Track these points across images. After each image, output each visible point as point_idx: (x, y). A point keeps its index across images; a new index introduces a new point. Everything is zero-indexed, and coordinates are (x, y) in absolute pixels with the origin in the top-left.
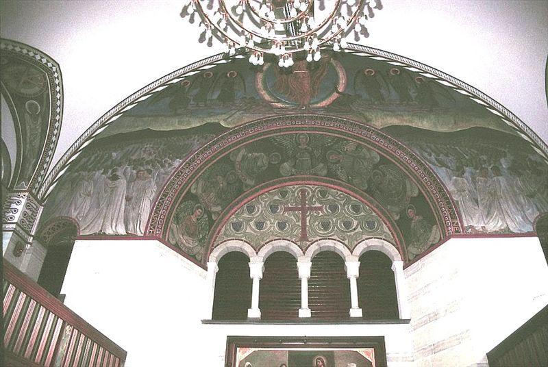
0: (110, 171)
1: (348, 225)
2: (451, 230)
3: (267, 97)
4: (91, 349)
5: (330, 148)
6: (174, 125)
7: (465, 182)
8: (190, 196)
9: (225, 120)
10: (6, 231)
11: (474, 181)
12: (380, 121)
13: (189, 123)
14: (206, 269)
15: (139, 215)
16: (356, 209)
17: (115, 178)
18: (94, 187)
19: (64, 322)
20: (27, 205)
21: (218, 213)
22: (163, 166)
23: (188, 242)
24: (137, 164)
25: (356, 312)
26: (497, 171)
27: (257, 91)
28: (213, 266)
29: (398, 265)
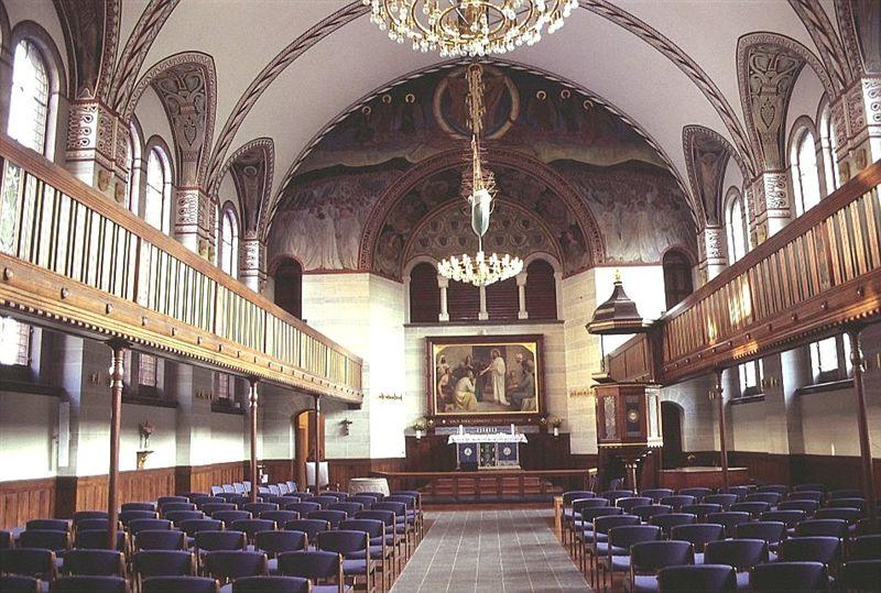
0: (316, 209)
1: (518, 240)
2: (596, 261)
3: (446, 128)
4: (240, 305)
5: (503, 175)
6: (363, 160)
7: (613, 217)
8: (387, 228)
9: (410, 155)
10: (85, 160)
11: (620, 217)
12: (548, 154)
13: (377, 157)
14: (401, 282)
15: (350, 251)
16: (526, 224)
17: (321, 216)
18: (306, 225)
19: (139, 238)
20: (101, 121)
21: (407, 234)
22: (361, 204)
23: (388, 265)
24: (337, 202)
25: (523, 315)
26: (642, 204)
27: (435, 120)
28: (407, 279)
29: (558, 275)
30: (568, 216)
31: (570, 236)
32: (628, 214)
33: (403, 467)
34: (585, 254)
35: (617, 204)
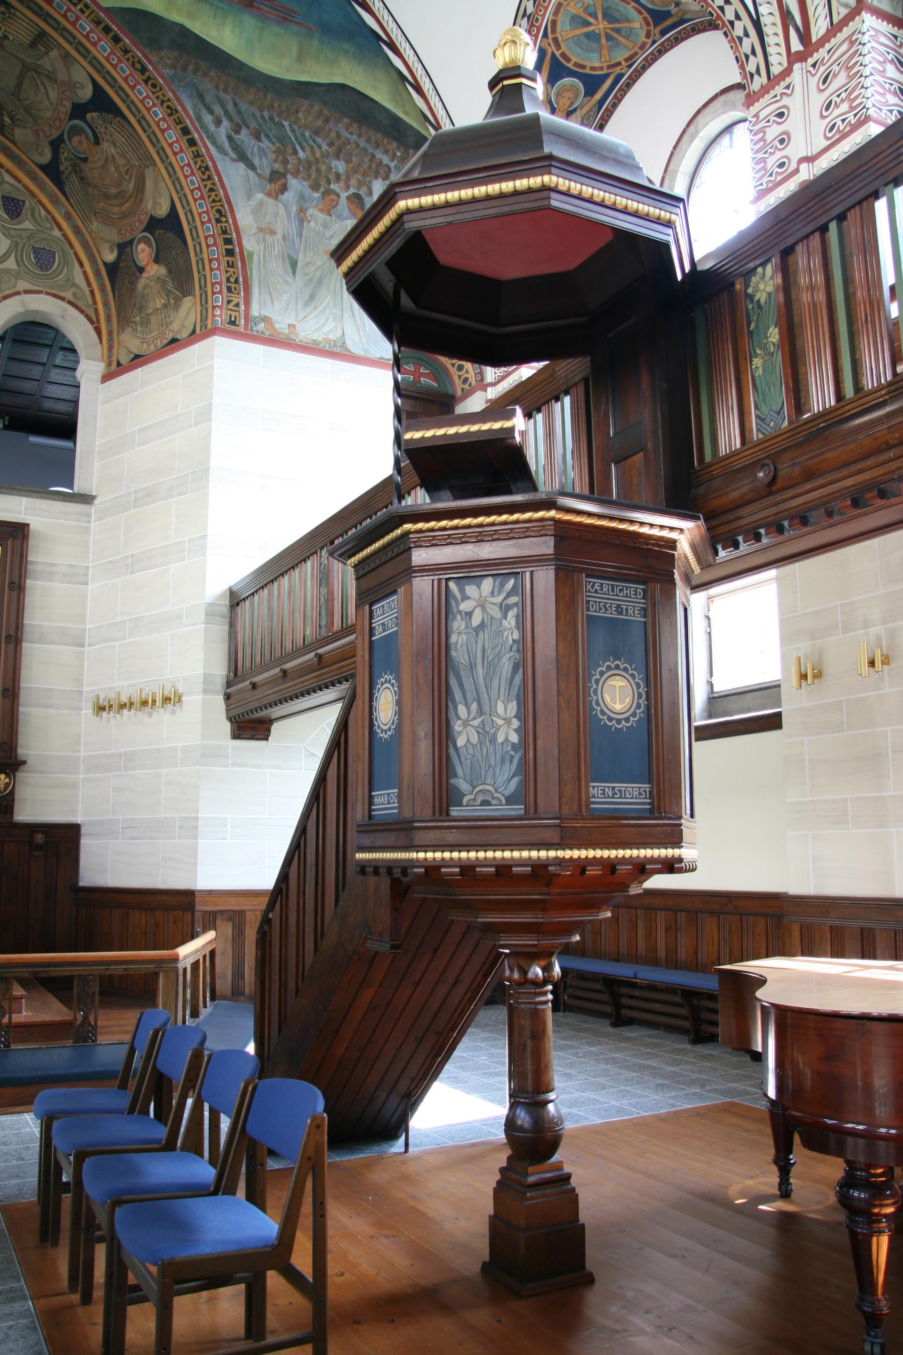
2: (220, 317)
11: (302, 217)
30: (149, 184)
31: (143, 253)
32: (322, 217)
33: (706, 714)
34: (187, 302)
35: (294, 183)
